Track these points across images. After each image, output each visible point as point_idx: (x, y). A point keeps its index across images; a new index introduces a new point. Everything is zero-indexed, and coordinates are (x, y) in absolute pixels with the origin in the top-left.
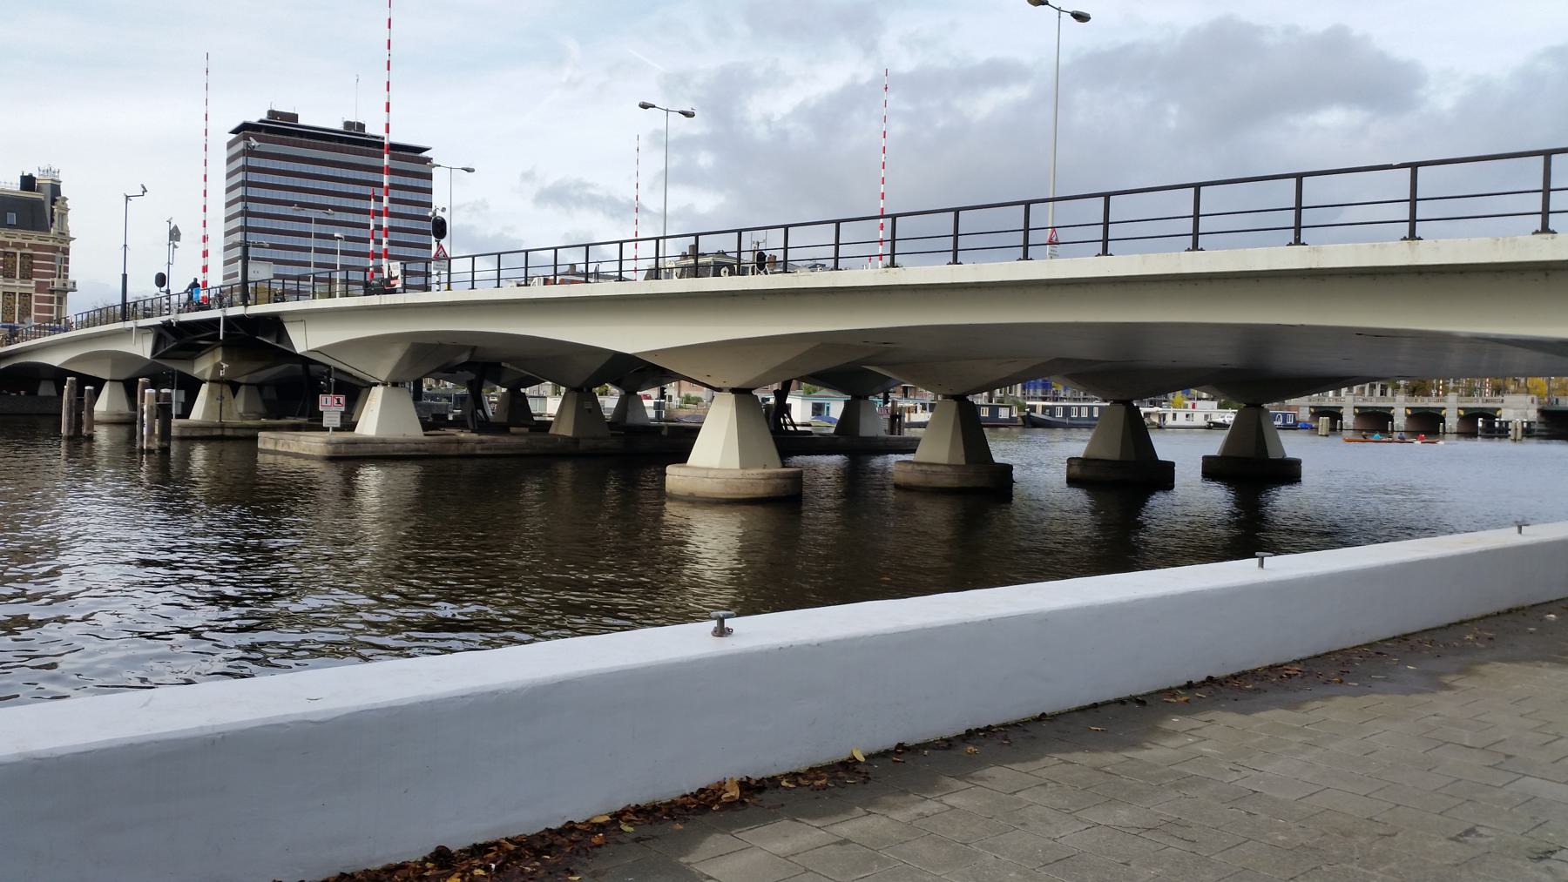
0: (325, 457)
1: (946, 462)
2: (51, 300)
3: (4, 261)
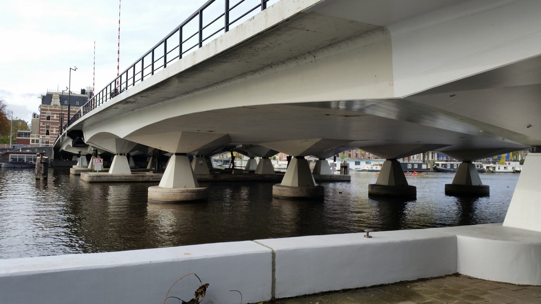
0: (88, 182)
1: (290, 185)
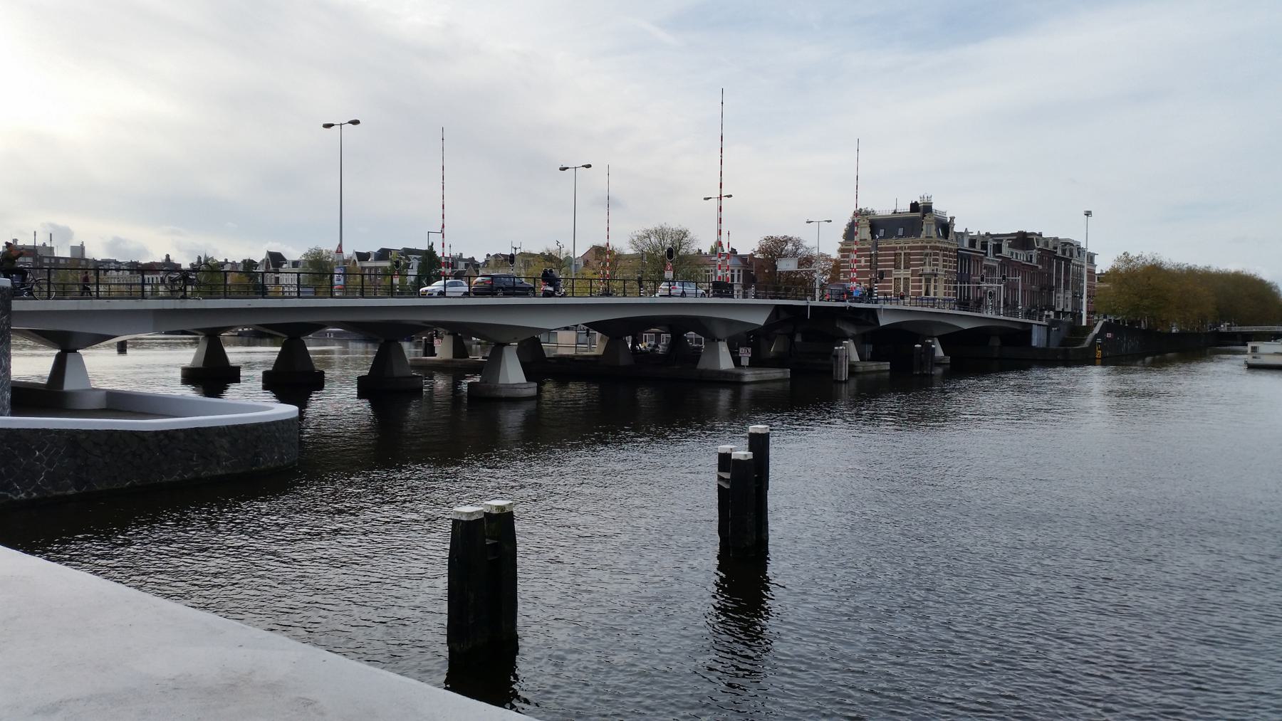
2: (920, 281)
3: (895, 259)
